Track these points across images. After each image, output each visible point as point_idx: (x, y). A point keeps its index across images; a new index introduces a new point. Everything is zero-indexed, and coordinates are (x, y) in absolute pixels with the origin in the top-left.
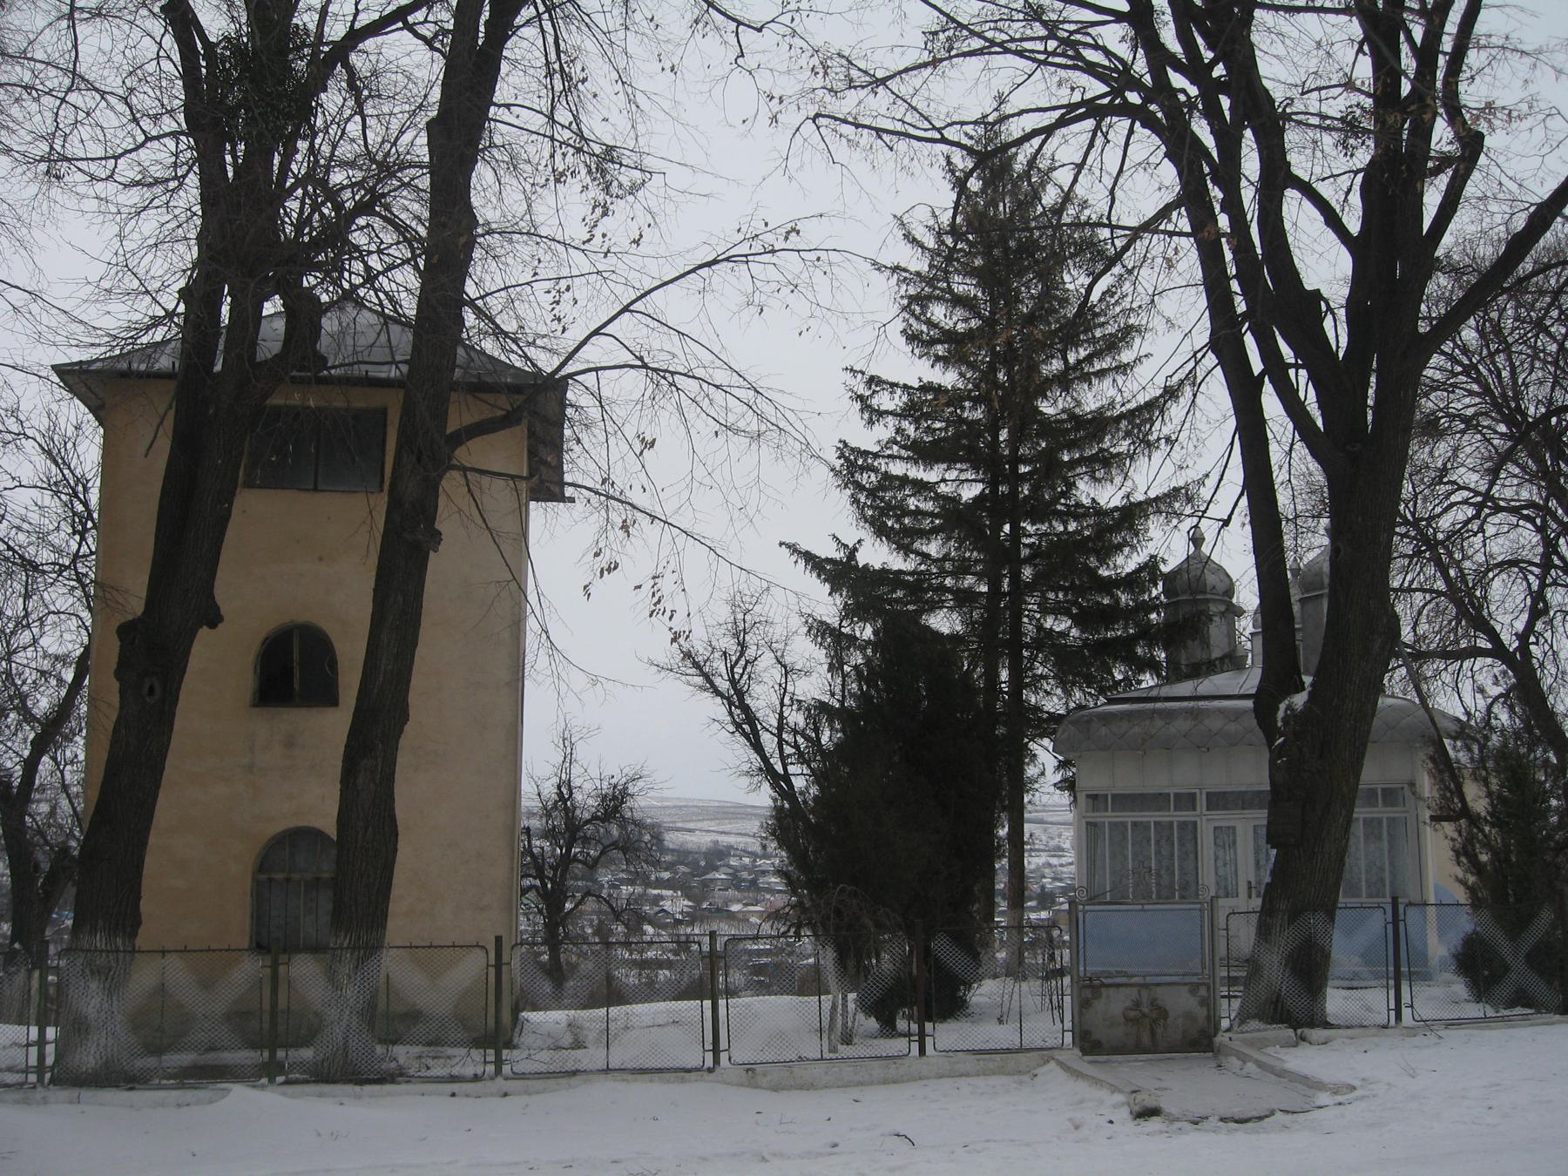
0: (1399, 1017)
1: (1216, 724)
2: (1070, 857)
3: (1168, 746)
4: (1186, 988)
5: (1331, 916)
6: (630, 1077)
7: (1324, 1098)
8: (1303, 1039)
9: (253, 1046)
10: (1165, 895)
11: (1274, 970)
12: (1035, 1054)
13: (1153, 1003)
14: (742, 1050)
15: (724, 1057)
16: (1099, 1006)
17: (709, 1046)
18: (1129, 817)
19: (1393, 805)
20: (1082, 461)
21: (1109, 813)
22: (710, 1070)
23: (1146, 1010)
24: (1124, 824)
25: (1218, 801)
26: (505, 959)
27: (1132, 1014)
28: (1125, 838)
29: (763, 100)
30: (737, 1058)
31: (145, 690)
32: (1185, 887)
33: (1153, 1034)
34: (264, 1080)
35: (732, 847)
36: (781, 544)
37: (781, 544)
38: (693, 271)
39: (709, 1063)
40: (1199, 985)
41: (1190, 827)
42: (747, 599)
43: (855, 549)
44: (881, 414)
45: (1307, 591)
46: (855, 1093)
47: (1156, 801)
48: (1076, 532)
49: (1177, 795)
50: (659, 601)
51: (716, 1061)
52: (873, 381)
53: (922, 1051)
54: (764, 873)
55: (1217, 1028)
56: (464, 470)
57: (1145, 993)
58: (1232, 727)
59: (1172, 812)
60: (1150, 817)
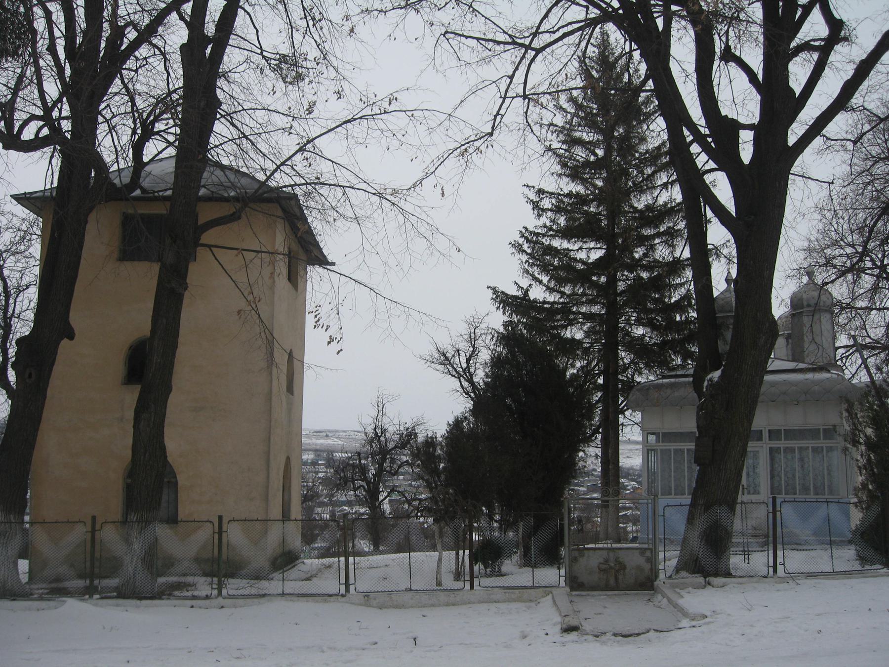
0: (775, 571)
4: (638, 551)
5: (732, 509)
6: (296, 599)
7: (685, 623)
8: (709, 584)
9: (81, 576)
11: (696, 543)
12: (541, 589)
13: (617, 561)
14: (364, 583)
15: (352, 588)
16: (583, 561)
17: (343, 581)
19: (830, 439)
20: (658, 235)
22: (343, 596)
23: (612, 565)
26: (224, 529)
27: (603, 567)
29: (427, 25)
30: (360, 589)
31: (27, 375)
33: (616, 579)
34: (87, 596)
36: (488, 287)
37: (488, 287)
38: (340, 125)
39: (343, 591)
40: (646, 549)
42: (476, 320)
43: (527, 290)
44: (544, 210)
46: (425, 611)
50: (318, 320)
51: (347, 590)
52: (540, 192)
53: (472, 587)
55: (657, 577)
56: (210, 246)
57: (611, 554)
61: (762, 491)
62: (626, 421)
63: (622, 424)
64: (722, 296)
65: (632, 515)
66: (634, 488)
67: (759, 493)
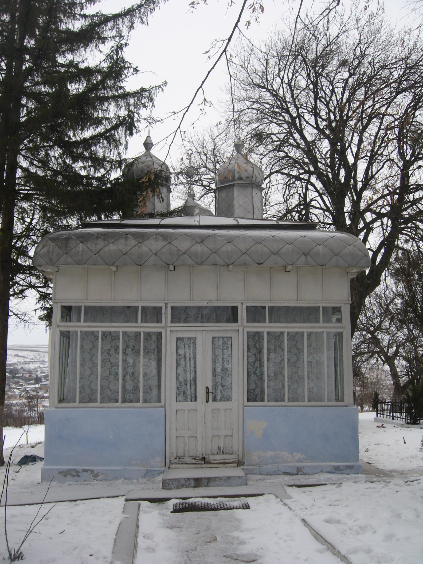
1: (184, 245)
2: (47, 365)
3: (140, 263)
10: (130, 397)
18: (100, 328)
21: (82, 323)
24: (94, 335)
25: (180, 314)
32: (148, 390)
41: (154, 338)
47: (128, 313)
48: (59, 183)
58: (199, 248)
59: (139, 324)
60: (120, 328)
67: (228, 399)
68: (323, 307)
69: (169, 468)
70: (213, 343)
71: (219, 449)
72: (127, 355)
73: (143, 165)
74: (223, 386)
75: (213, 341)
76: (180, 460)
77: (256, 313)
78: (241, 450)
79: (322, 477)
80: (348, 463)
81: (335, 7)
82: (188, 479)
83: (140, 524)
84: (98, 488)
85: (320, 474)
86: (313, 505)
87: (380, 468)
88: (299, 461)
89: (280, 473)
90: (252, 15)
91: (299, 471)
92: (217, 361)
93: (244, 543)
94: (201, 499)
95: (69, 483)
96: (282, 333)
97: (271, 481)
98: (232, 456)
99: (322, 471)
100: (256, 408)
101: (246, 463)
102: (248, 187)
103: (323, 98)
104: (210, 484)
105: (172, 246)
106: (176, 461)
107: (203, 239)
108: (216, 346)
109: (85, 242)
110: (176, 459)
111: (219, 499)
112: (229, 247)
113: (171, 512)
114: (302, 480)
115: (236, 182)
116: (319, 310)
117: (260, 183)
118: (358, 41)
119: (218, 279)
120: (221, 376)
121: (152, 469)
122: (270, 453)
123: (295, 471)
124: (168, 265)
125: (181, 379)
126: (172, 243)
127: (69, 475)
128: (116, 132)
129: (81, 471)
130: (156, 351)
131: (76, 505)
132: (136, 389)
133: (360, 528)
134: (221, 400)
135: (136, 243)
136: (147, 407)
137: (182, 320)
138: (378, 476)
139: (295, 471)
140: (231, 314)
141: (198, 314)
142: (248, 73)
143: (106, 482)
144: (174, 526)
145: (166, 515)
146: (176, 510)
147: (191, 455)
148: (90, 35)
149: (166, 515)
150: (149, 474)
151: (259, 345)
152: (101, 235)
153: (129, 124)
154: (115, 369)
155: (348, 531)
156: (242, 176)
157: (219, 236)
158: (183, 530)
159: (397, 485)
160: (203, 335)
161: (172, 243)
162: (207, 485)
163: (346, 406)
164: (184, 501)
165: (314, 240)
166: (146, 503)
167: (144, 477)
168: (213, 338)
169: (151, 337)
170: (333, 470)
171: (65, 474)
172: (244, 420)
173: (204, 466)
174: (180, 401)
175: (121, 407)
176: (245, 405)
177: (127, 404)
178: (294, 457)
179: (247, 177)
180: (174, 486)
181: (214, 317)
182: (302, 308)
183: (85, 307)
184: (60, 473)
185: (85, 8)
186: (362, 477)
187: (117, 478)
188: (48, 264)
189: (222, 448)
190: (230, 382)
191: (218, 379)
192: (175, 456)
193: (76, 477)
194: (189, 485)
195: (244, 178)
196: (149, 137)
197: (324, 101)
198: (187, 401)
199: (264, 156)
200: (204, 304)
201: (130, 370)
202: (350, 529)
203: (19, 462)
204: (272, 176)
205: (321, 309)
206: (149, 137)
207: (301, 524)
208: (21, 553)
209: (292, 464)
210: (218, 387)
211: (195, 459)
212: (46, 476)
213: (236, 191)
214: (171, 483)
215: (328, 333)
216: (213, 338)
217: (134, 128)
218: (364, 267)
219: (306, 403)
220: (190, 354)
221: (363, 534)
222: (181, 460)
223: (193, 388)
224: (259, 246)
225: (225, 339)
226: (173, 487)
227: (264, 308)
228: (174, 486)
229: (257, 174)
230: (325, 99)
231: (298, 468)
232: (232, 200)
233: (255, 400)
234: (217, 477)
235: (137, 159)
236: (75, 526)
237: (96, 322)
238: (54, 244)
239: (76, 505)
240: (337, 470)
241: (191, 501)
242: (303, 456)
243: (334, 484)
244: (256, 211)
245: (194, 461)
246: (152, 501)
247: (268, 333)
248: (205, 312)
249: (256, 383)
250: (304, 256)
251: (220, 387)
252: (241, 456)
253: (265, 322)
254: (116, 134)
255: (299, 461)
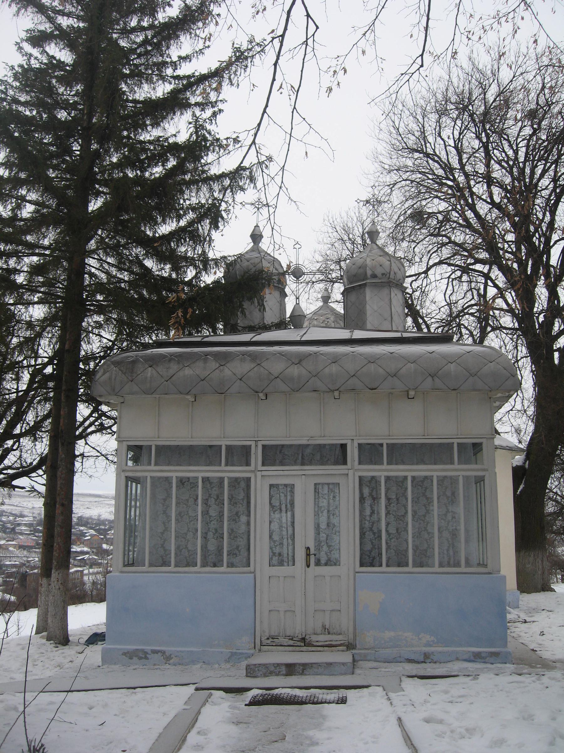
1: (277, 367)
3: (221, 391)
10: (213, 560)
18: (175, 472)
24: (168, 480)
25: (275, 455)
28: (169, 496)
35: (4, 511)
41: (243, 484)
45: (351, 283)
47: (208, 453)
49: (229, 448)
54: (19, 525)
58: (295, 371)
60: (199, 472)
61: (344, 559)
62: (87, 450)
63: (82, 455)
64: (247, 256)
65: (89, 559)
66: (92, 536)
67: (336, 563)
68: (458, 443)
69: (260, 650)
70: (315, 491)
71: (324, 627)
72: (210, 506)
73: (249, 263)
74: (329, 546)
75: (315, 488)
76: (273, 641)
77: (370, 453)
78: (351, 630)
79: (455, 667)
80: (494, 649)
81: (418, 69)
82: (278, 665)
83: (200, 718)
84: (170, 673)
85: (454, 663)
86: (426, 701)
87: (544, 657)
88: (428, 645)
89: (402, 660)
90: (333, 79)
91: (426, 658)
92: (321, 514)
93: (317, 744)
94: (290, 689)
95: (135, 667)
96: (406, 478)
97: (387, 670)
98: (340, 637)
99: (457, 659)
100: (372, 575)
101: (358, 646)
102: (384, 286)
103: (505, 161)
104: (305, 672)
105: (262, 369)
106: (269, 641)
107: (300, 359)
108: (320, 495)
109: (154, 366)
110: (268, 639)
111: (312, 690)
112: (334, 368)
113: (246, 705)
114: (429, 670)
115: (368, 281)
116: (453, 448)
117: (401, 281)
118: (541, 86)
119: (322, 410)
120: (326, 533)
121: (238, 651)
122: (389, 634)
123: (421, 658)
124: (257, 392)
125: (276, 537)
126: (262, 364)
127: (136, 656)
128: (199, 225)
129: (149, 652)
130: (245, 501)
131: (133, 693)
132: (220, 550)
133: (467, 730)
134: (326, 564)
135: (218, 365)
136: (233, 573)
137: (278, 461)
138: (532, 667)
139: (421, 658)
140: (340, 454)
141: (298, 454)
142: (400, 135)
143: (180, 667)
144: (241, 721)
145: (239, 709)
146: (254, 702)
147: (288, 634)
148: (174, 103)
149: (239, 709)
150: (233, 658)
151: (377, 494)
152: (175, 356)
153: (213, 214)
154: (194, 524)
155: (448, 733)
156: (376, 273)
157: (322, 354)
158: (251, 726)
159: (553, 679)
160: (302, 480)
161: (262, 364)
162: (302, 673)
163: (490, 573)
164: (268, 692)
165: (444, 356)
166: (221, 693)
167: (227, 661)
168: (315, 484)
169: (239, 483)
170: (472, 658)
171: (130, 655)
172: (355, 590)
173: (305, 648)
174: (273, 566)
175: (199, 573)
176: (357, 570)
177: (208, 569)
178: (420, 639)
179: (383, 274)
180: (261, 673)
181: (318, 458)
182: (432, 444)
183: (156, 446)
184: (125, 654)
185: (179, 67)
186: (510, 667)
187: (193, 662)
188: (110, 394)
189: (327, 627)
190: (338, 542)
191: (323, 537)
192: (267, 634)
193: (143, 660)
194: (279, 672)
195: (379, 275)
196: (257, 226)
197: (506, 165)
198: (283, 565)
199: (418, 243)
200: (304, 442)
201: (213, 525)
202: (452, 732)
203: (86, 641)
204: (425, 269)
205: (455, 446)
206: (257, 226)
207: (396, 722)
208: (42, 745)
209: (418, 649)
210: (322, 547)
211: (292, 639)
212: (107, 659)
213: (369, 293)
214: (256, 669)
215: (466, 478)
216: (315, 484)
217: (220, 219)
218: (510, 391)
219: (437, 569)
220: (286, 506)
221: (470, 738)
222: (274, 640)
223: (290, 548)
224: (372, 367)
225: (331, 486)
226: (259, 675)
227: (381, 445)
228: (261, 673)
229: (396, 270)
230: (507, 162)
231: (425, 653)
232: (363, 303)
233: (372, 565)
234: (315, 663)
235: (240, 256)
236: (123, 717)
237: (171, 465)
238: (118, 370)
239: (133, 693)
240: (477, 657)
241: (276, 692)
242: (432, 638)
243: (468, 676)
244: (395, 318)
245: (291, 642)
246: (228, 690)
247: (388, 479)
248: (308, 451)
249: (372, 543)
250: (430, 379)
251: (325, 548)
252: (351, 636)
253: (383, 464)
254: (200, 228)
255: (428, 645)
